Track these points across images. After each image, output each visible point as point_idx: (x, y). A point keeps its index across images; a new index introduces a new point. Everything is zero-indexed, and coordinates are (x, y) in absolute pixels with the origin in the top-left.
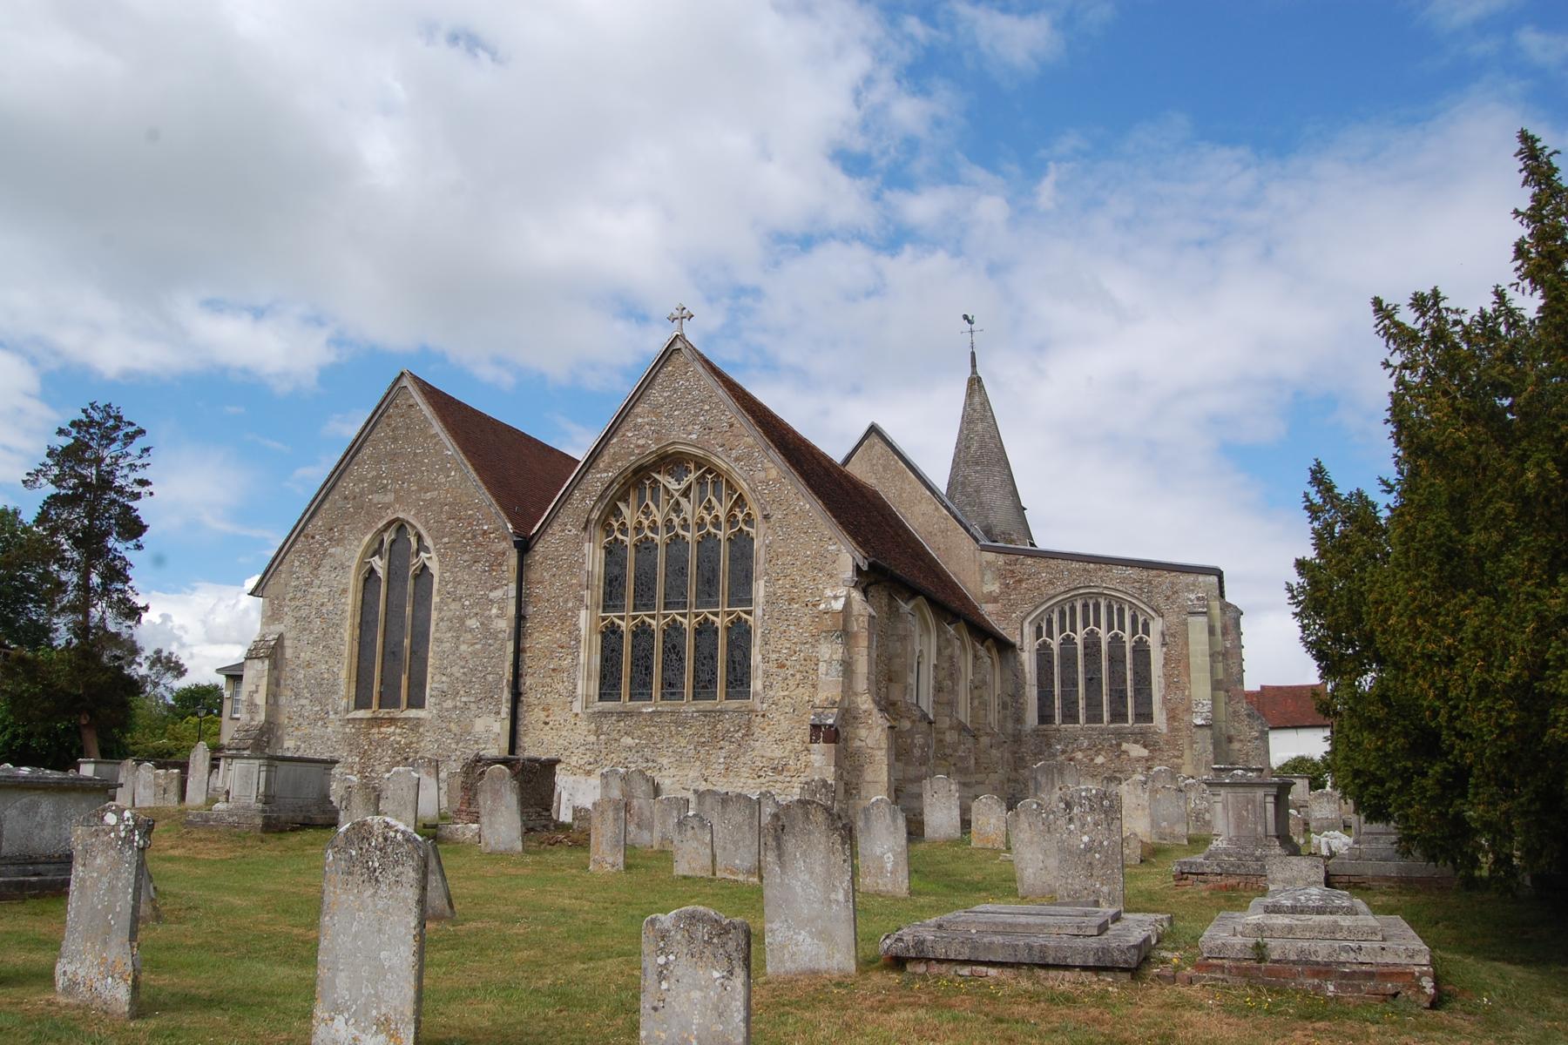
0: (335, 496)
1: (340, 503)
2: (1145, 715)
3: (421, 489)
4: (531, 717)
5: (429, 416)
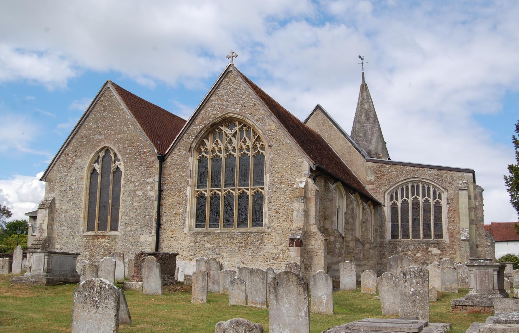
0: (78, 136)
1: (80, 140)
2: (439, 235)
4: (165, 235)
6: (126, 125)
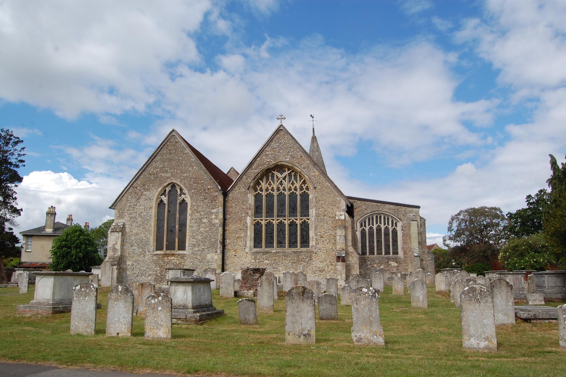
0: (145, 173)
1: (148, 176)
2: (395, 252)
3: (182, 172)
5: (185, 146)
6: (191, 165)
